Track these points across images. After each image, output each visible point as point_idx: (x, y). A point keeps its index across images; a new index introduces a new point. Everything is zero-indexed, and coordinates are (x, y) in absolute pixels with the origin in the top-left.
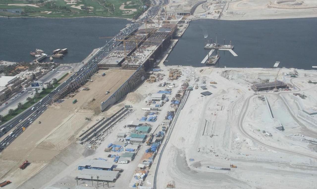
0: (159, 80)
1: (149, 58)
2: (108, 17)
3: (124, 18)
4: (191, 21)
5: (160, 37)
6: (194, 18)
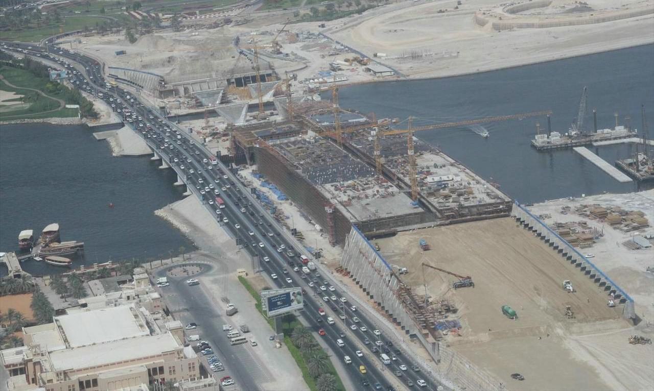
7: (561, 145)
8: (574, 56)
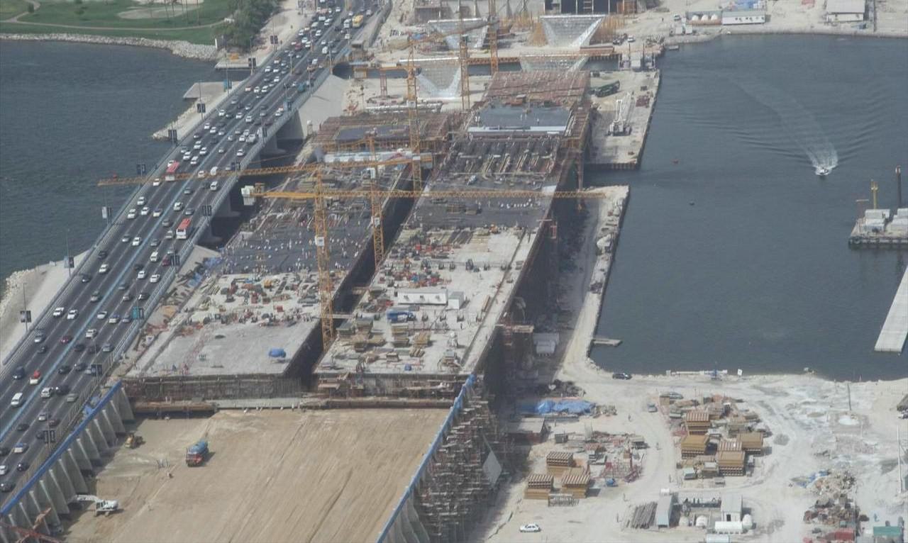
0: (619, 481)
1: (502, 319)
2: (15, 37)
3: (144, 41)
4: (664, 50)
5: (510, 168)
6: (679, 31)
7: (899, 239)
8: (763, 32)
